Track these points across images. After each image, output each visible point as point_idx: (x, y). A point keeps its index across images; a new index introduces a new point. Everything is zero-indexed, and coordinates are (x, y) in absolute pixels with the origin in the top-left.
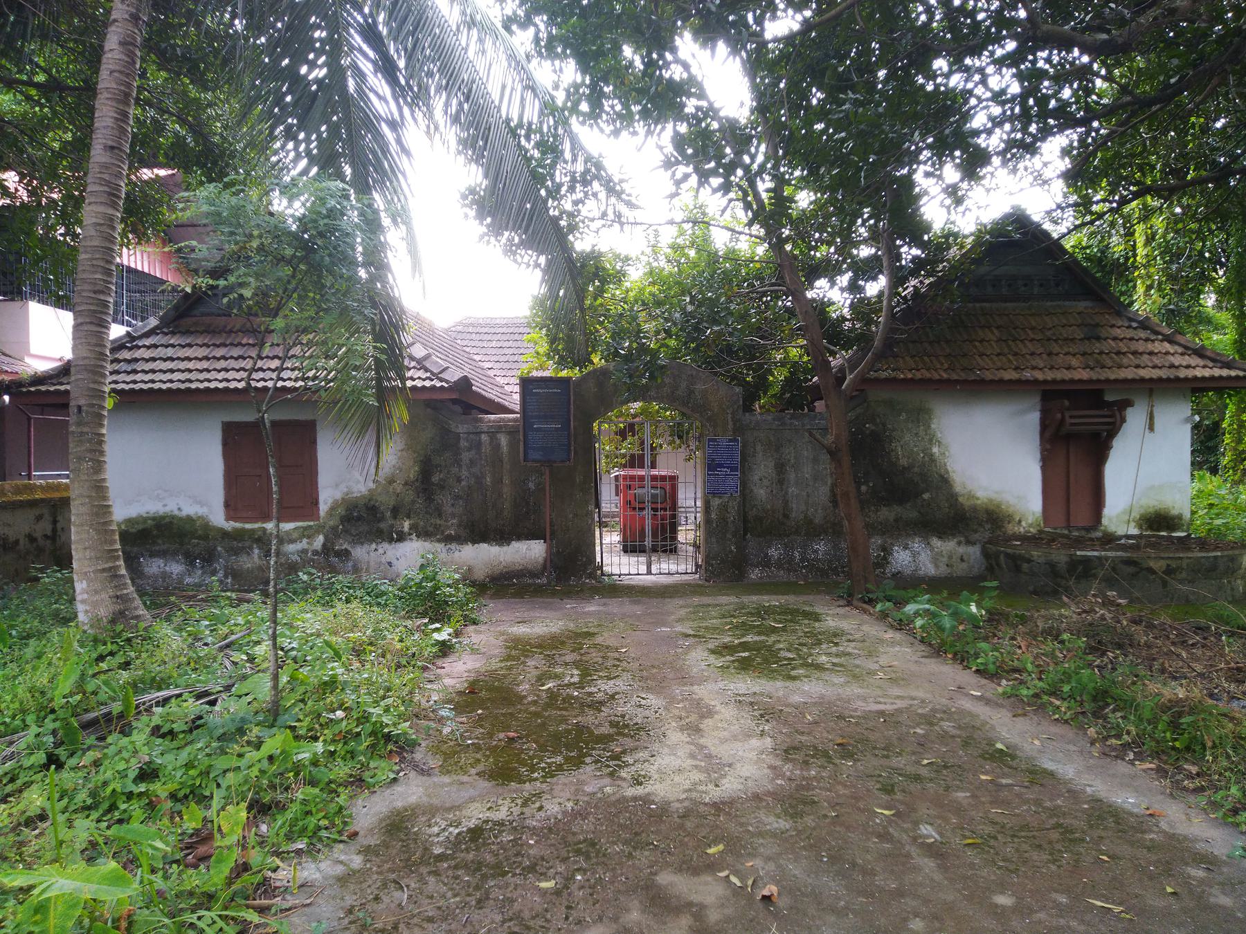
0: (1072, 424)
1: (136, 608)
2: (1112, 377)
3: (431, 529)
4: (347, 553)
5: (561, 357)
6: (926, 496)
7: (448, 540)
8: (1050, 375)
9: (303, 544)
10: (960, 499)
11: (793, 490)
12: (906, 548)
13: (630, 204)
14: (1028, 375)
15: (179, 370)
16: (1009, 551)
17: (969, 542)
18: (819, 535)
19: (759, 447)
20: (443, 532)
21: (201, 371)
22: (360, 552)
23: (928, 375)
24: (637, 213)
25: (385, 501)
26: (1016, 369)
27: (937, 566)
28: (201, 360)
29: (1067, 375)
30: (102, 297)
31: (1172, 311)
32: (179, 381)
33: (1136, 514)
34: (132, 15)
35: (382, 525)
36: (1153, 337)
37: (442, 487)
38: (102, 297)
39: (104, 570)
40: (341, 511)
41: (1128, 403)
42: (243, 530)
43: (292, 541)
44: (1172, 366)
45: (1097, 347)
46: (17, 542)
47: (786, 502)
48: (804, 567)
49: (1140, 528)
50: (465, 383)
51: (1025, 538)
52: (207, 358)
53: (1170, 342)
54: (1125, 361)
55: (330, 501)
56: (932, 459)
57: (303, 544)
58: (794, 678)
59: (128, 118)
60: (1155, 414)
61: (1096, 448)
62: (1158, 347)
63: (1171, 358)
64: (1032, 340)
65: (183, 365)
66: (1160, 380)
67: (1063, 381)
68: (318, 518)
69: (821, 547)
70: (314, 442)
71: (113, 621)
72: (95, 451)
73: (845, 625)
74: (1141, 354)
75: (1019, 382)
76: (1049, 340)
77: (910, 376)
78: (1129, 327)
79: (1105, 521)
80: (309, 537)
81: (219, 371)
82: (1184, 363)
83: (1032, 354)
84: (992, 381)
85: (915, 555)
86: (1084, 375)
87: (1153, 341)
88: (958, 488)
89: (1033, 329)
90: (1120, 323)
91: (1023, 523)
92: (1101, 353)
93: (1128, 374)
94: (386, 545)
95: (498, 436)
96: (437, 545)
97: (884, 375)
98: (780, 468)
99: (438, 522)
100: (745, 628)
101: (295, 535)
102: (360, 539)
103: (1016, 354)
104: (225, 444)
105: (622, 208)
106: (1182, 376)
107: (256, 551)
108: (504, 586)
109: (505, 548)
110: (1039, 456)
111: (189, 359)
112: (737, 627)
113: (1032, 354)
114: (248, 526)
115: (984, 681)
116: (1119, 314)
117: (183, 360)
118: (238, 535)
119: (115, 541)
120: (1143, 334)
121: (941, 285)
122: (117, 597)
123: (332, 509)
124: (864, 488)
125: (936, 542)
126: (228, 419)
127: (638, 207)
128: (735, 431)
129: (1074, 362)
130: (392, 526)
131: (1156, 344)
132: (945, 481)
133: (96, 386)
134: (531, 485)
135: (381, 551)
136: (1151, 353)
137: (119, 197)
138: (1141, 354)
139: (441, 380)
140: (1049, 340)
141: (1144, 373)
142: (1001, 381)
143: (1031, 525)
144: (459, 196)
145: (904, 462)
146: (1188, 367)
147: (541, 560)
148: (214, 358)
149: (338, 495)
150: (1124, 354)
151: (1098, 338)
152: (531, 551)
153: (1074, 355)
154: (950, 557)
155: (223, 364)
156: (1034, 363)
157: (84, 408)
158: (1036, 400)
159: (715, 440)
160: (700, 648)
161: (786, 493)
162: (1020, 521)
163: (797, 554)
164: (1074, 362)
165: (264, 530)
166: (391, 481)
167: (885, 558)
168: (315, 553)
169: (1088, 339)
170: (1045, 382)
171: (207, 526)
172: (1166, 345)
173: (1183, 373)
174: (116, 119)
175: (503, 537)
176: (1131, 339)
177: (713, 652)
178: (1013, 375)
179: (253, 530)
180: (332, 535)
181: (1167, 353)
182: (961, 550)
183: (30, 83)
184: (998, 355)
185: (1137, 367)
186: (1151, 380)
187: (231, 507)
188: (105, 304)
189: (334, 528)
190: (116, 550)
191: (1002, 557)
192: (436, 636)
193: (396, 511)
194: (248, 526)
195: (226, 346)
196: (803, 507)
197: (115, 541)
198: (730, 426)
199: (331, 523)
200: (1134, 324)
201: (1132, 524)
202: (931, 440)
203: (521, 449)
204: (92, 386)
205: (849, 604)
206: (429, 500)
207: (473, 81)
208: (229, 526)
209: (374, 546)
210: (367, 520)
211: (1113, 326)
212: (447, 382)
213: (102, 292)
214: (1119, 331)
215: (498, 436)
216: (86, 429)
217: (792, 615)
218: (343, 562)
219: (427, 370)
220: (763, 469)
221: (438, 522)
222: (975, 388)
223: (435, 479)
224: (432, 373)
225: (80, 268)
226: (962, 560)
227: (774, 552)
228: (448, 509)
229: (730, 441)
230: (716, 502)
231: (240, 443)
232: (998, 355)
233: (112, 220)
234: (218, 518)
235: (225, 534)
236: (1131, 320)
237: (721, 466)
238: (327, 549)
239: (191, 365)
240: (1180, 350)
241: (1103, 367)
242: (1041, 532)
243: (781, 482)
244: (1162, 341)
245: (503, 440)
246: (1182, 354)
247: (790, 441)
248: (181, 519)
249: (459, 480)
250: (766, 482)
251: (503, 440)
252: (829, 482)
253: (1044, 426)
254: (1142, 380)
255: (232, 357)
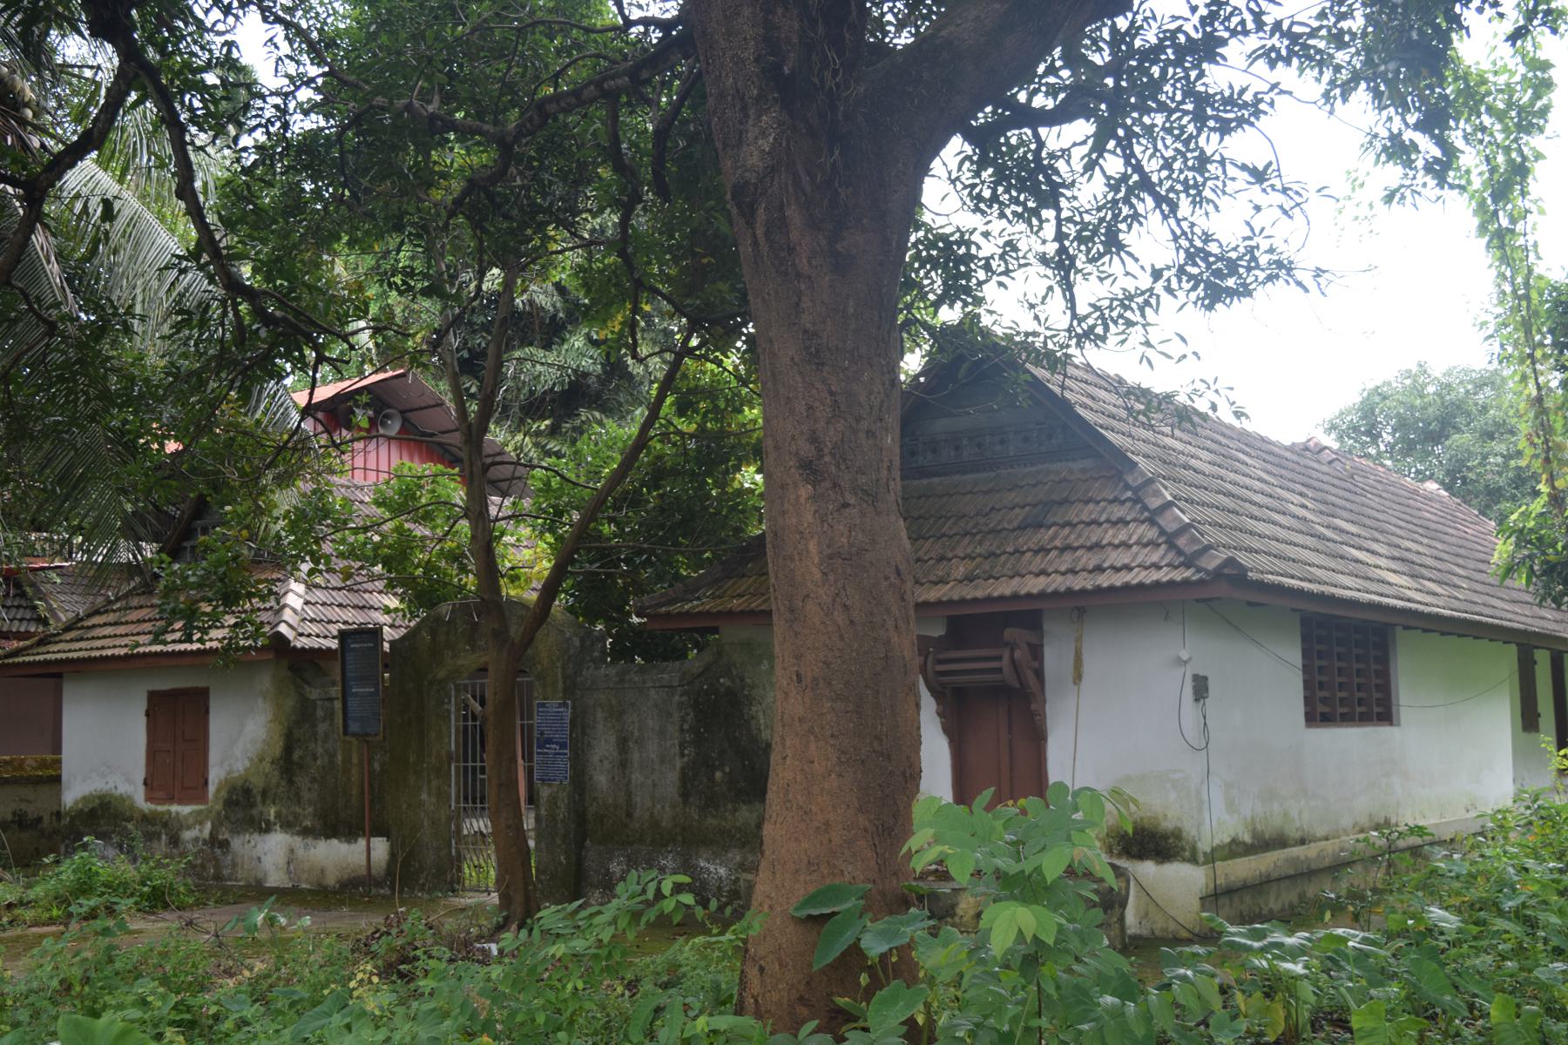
7: (306, 832)
11: (637, 777)
18: (666, 846)
19: (600, 715)
25: (257, 783)
37: (301, 767)
46: (39, 819)
47: (629, 795)
70: (207, 712)
94: (256, 836)
98: (623, 743)
114: (160, 808)
124: (718, 775)
128: (565, 690)
161: (629, 782)
183: (31, 309)
196: (649, 804)
198: (560, 686)
206: (291, 782)
208: (146, 807)
220: (603, 747)
223: (296, 756)
228: (306, 795)
229: (560, 705)
243: (624, 764)
247: (632, 704)
249: (315, 758)
250: (607, 765)
252: (678, 765)
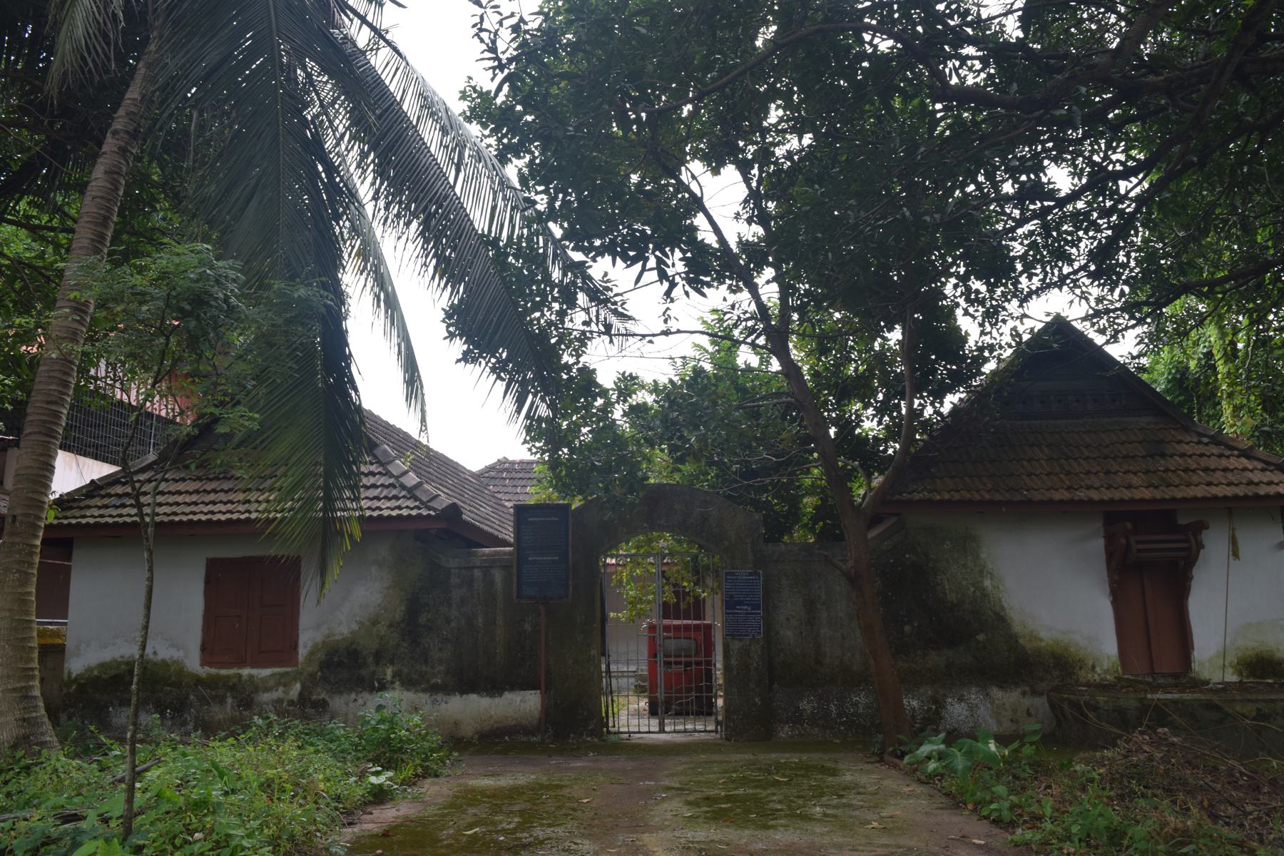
0: (1139, 551)
1: (43, 734)
2: (1179, 495)
3: (416, 677)
4: (324, 704)
5: (564, 485)
6: (981, 637)
7: (433, 689)
8: (1107, 495)
9: (278, 693)
10: (1021, 641)
12: (961, 699)
13: (624, 317)
14: (1081, 494)
15: (167, 504)
16: (1073, 697)
17: (1035, 693)
20: (428, 682)
21: (189, 505)
22: (337, 703)
23: (968, 496)
24: (630, 326)
26: (1069, 488)
27: (999, 722)
28: (191, 493)
29: (1127, 495)
30: (54, 407)
31: (1268, 434)
32: (165, 514)
33: (1232, 658)
34: (120, 148)
35: (364, 672)
36: (1227, 453)
38: (54, 407)
39: (15, 690)
40: (321, 656)
41: (1199, 527)
42: (218, 676)
43: (267, 690)
44: (1250, 483)
45: (1162, 464)
48: (841, 723)
49: (1240, 674)
50: (453, 512)
51: (1102, 687)
52: (197, 492)
53: (1249, 457)
54: (1195, 478)
55: (310, 644)
56: (985, 595)
57: (278, 693)
58: (768, 828)
59: (104, 239)
60: (1237, 535)
61: (1175, 580)
62: (1233, 463)
63: (1250, 475)
64: (1087, 458)
65: (171, 499)
66: (1236, 498)
67: (1122, 501)
68: (296, 664)
69: (861, 699)
70: (298, 579)
71: (15, 747)
72: (24, 562)
73: (864, 779)
74: (1214, 471)
75: (1072, 502)
76: (1106, 458)
77: (947, 497)
78: (1199, 443)
79: (1196, 666)
80: (285, 686)
81: (207, 504)
82: (1265, 480)
83: (1088, 473)
84: (1041, 502)
85: (972, 708)
86: (1147, 494)
87: (1228, 457)
88: (1017, 628)
89: (1088, 446)
90: (1189, 439)
91: (1098, 669)
92: (1167, 470)
93: (1200, 492)
94: (366, 695)
95: (492, 571)
96: (421, 695)
97: (917, 496)
99: (424, 668)
100: (744, 782)
101: (271, 683)
102: (341, 687)
103: (1068, 473)
104: (207, 582)
105: (613, 320)
106: (1262, 493)
107: (229, 700)
108: (495, 742)
109: (497, 700)
110: (1108, 589)
111: (179, 493)
112: (733, 782)
113: (1088, 473)
114: (223, 672)
115: (996, 831)
116: (1186, 429)
117: (174, 494)
118: (211, 683)
119: (32, 660)
120: (1216, 450)
121: (978, 400)
122: (24, 720)
123: (312, 653)
125: (997, 693)
126: (211, 555)
127: (630, 318)
129: (1135, 480)
130: (374, 673)
131: (1232, 460)
132: (1001, 620)
133: (35, 496)
134: (528, 627)
135: (360, 701)
136: (1225, 470)
137: (86, 313)
138: (1214, 471)
139: (429, 508)
140: (1106, 458)
141: (1220, 491)
142: (1051, 502)
143: (1106, 671)
144: (443, 315)
145: (952, 597)
146: (1270, 483)
147: (537, 714)
148: (205, 491)
149: (319, 638)
150: (1193, 471)
151: (1163, 455)
152: (524, 704)
153: (1135, 473)
154: (1014, 711)
155: (212, 497)
156: (1089, 483)
157: (19, 518)
158: (1099, 525)
159: (733, 574)
160: (677, 799)
162: (1094, 667)
163: (833, 708)
164: (1135, 480)
165: (240, 676)
166: (375, 622)
167: (937, 712)
168: (291, 703)
169: (1152, 456)
170: (1102, 502)
171: (181, 672)
172: (1243, 460)
173: (1262, 491)
174: (93, 240)
175: (494, 687)
176: (1202, 455)
177: (689, 803)
178: (1065, 495)
179: (228, 677)
180: (310, 683)
181: (1245, 469)
182: (1027, 702)
184: (1048, 474)
185: (1209, 484)
186: (1225, 498)
187: (208, 651)
188: (57, 415)
189: (312, 675)
190: (32, 669)
191: (1066, 706)
192: (373, 780)
193: (378, 656)
194: (223, 672)
195: (219, 479)
197: (32, 660)
199: (310, 669)
200: (1205, 440)
201: (1230, 670)
202: (981, 572)
203: (515, 585)
204: (30, 495)
205: (881, 761)
207: (446, 197)
209: (353, 696)
210: (348, 667)
211: (1180, 442)
212: (434, 510)
213: (55, 403)
214: (1187, 447)
215: (492, 571)
216: (17, 540)
217: (807, 769)
218: (319, 713)
219: (416, 499)
220: (790, 608)
221: (424, 668)
222: (1029, 512)
223: (423, 619)
224: (422, 502)
225: (37, 380)
226: (1029, 714)
227: (806, 706)
229: (750, 574)
230: (736, 645)
231: (218, 578)
232: (1048, 474)
233: (75, 334)
234: (193, 663)
235: (199, 681)
236: (1200, 435)
237: (741, 603)
238: (303, 699)
239: (180, 499)
240: (1260, 465)
241: (1169, 485)
242: (1119, 679)
244: (1238, 457)
245: (498, 576)
246: (1263, 470)
248: (155, 664)
249: (448, 621)
251: (498, 576)
253: (1110, 555)
254: (1215, 498)
255: (222, 490)
